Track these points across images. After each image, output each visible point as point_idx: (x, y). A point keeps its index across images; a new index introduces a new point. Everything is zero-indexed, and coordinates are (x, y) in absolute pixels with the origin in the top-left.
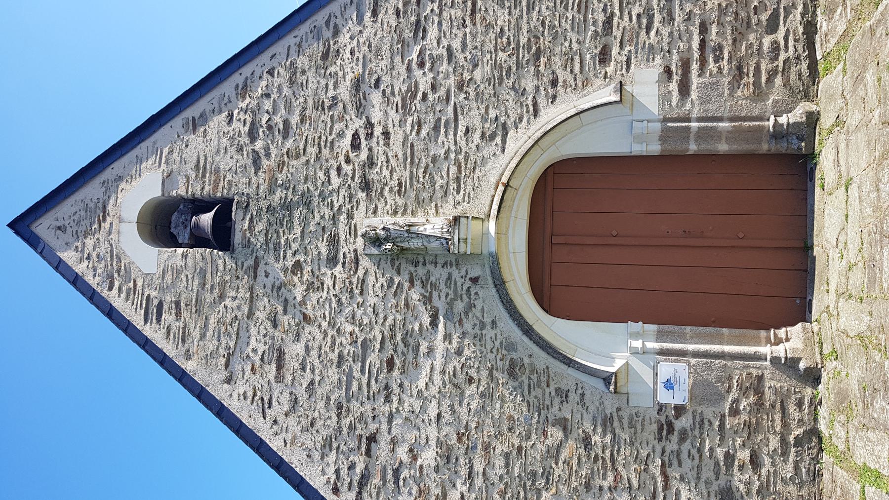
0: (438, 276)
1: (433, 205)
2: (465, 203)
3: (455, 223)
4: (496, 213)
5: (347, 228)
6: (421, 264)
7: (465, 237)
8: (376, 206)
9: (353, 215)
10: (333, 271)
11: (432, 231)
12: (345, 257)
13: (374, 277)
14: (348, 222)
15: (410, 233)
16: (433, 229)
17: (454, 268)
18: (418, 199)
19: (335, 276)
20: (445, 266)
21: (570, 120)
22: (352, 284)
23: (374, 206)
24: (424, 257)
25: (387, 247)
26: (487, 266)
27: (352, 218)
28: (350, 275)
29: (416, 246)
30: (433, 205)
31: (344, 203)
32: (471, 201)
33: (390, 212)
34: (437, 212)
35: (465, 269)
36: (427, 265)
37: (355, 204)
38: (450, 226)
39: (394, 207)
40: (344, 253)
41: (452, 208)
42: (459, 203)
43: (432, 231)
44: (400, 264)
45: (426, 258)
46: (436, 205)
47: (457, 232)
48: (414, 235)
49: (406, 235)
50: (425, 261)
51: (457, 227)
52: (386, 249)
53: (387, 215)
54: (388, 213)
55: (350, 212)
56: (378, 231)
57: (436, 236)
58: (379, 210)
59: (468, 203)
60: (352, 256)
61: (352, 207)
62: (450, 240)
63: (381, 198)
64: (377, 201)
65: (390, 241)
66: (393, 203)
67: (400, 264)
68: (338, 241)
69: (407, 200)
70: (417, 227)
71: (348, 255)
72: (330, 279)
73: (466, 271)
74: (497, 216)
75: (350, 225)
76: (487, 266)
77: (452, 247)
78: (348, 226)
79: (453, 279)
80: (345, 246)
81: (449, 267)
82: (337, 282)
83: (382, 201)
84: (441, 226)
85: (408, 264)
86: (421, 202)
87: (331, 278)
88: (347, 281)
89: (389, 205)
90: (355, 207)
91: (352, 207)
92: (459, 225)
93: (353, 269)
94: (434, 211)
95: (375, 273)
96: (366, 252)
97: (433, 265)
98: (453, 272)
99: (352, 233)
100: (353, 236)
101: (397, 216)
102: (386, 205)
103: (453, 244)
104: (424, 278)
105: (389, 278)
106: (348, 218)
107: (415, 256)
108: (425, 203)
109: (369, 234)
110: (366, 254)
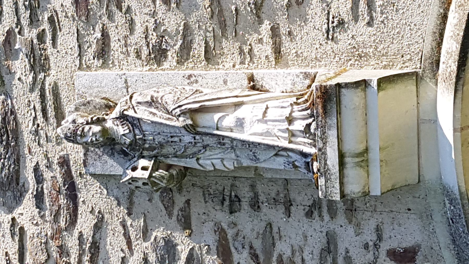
0: (297, 241)
1: (266, 27)
2: (362, 23)
3: (324, 108)
4: (454, 67)
5: (35, 96)
6: (245, 205)
7: (361, 147)
8: (105, 35)
9: (47, 58)
10: (16, 214)
11: (261, 128)
12: (39, 179)
13: (122, 238)
14: (35, 79)
15: (198, 133)
16: (264, 119)
17: (341, 219)
18: (221, 11)
19: (22, 229)
20: (316, 213)
21: (422, 142)
22: (68, 255)
23: (99, 35)
24: (253, 187)
25: (139, 174)
26: (437, 217)
27: (45, 68)
28: (59, 231)
29: (219, 166)
30: (266, 27)
31: (18, 23)
32: (378, 17)
33: (145, 52)
34: (277, 51)
35: (372, 224)
36: (265, 208)
37: (46, 26)
38: (312, 116)
39: (153, 38)
40: (36, 169)
41: (322, 38)
42: (341, 23)
43: (261, 128)
44: (188, 202)
45: (260, 188)
46: (275, 32)
47: (332, 135)
48: (208, 140)
49: (188, 138)
50: (256, 195)
51: (333, 121)
52: (134, 180)
53: (139, 62)
54: (138, 56)
55: (38, 52)
56: (109, 124)
57: (273, 147)
58: (114, 45)
59: (369, 24)
60: (58, 176)
61: (41, 37)
62: (314, 158)
63: (114, 8)
64: (105, 18)
65: (145, 153)
66: (151, 26)
67: (188, 202)
68: (17, 133)
69: (187, 15)
70: (217, 116)
71: (47, 175)
72: (8, 236)
73: (378, 230)
74: (458, 78)
75: (42, 90)
76: (437, 217)
77: (322, 181)
78: (36, 93)
79: (341, 251)
80: (35, 148)
81: (327, 217)
82: (28, 244)
83: (119, 17)
84: (287, 112)
85: (210, 204)
86: (229, 23)
87: (13, 235)
88: (53, 246)
89: (139, 29)
90: (49, 37)
91: (41, 37)
92: (339, 113)
93: (64, 213)
94: (268, 49)
95: (124, 226)
96: (92, 170)
97: (281, 209)
98: (339, 230)
99: (51, 112)
100: (52, 120)
101: (166, 65)
102: (132, 30)
103: (325, 172)
104: (258, 244)
105: (162, 243)
106: (32, 68)
107: (228, 183)
108: (240, 26)
109: (83, 135)
110: (94, 175)
